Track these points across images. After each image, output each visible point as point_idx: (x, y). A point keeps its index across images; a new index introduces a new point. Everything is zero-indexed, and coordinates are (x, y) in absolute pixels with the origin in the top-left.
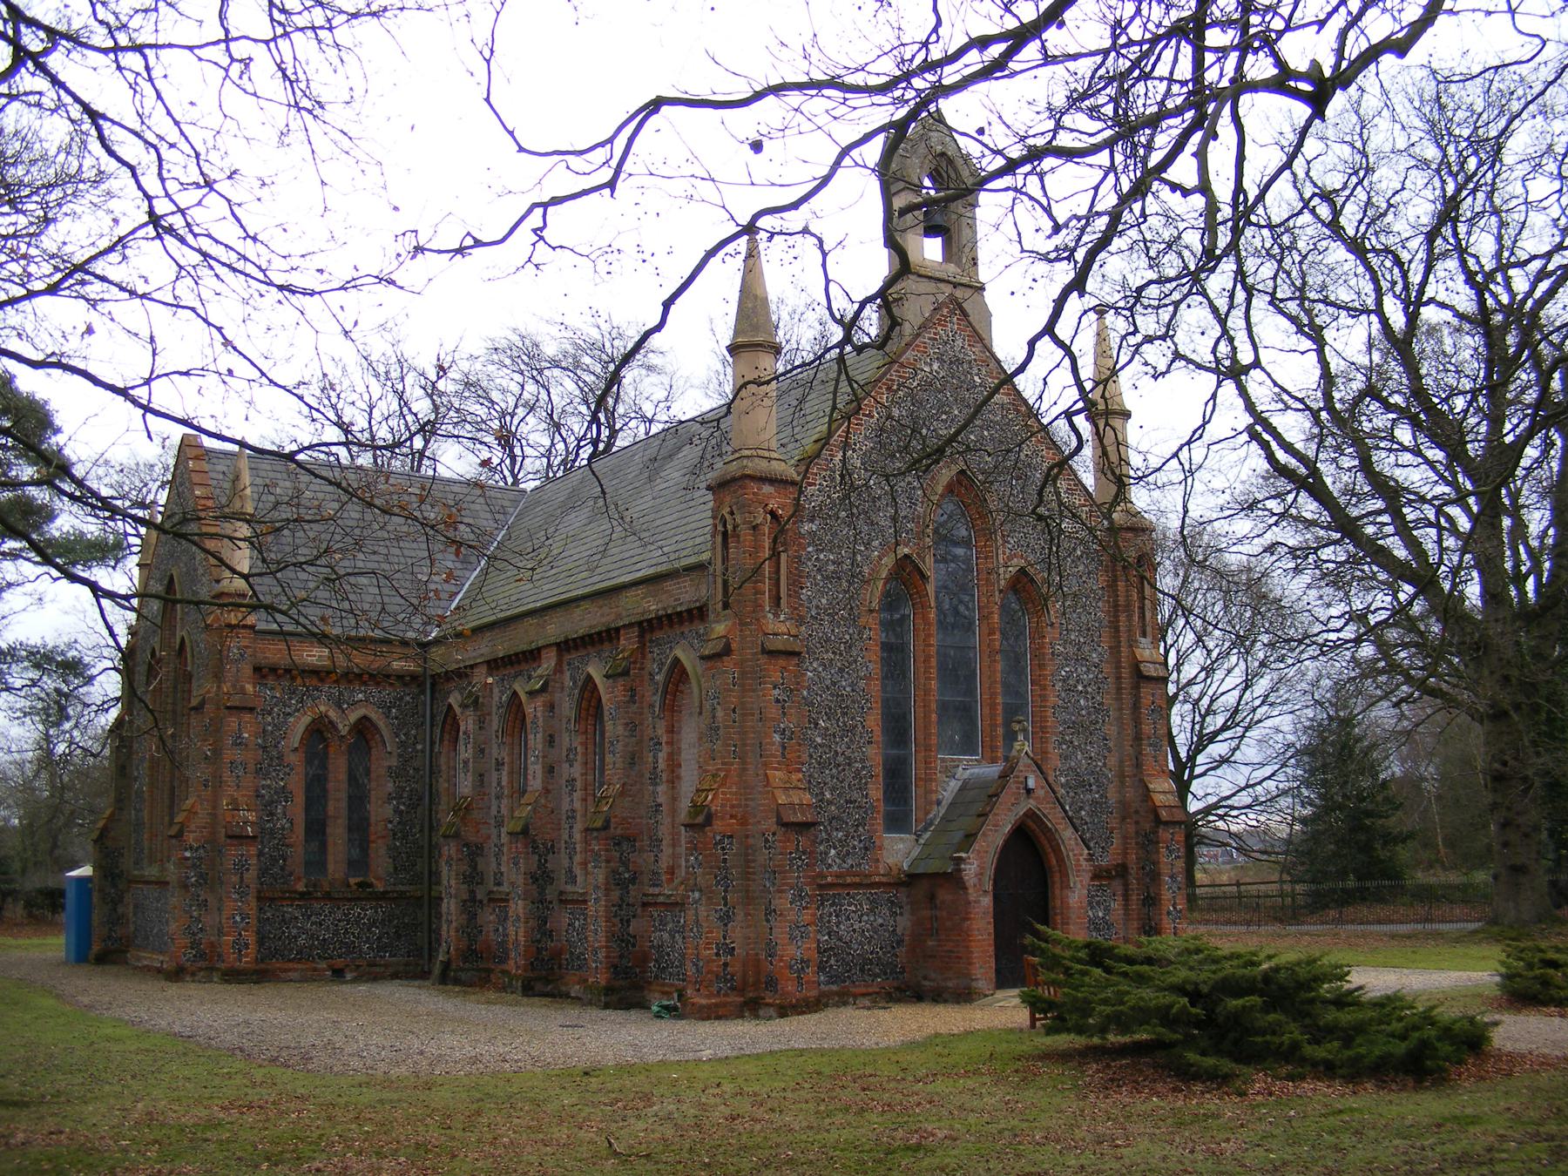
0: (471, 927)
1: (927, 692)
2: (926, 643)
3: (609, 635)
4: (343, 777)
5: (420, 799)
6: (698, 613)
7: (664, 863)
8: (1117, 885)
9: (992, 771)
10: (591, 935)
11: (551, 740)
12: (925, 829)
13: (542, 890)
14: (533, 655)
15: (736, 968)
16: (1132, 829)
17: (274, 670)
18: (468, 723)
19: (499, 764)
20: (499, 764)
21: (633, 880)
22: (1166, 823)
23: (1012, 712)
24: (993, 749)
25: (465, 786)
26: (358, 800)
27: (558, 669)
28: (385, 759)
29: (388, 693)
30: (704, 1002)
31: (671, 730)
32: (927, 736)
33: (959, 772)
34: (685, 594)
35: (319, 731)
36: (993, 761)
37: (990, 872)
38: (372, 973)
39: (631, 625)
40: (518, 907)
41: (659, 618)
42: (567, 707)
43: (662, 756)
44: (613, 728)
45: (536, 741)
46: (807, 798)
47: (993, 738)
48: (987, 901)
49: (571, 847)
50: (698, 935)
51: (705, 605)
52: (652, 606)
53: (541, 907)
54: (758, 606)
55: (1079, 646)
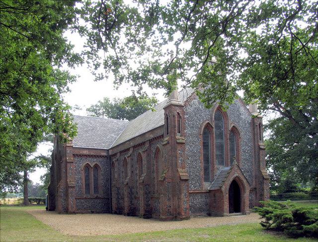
0: (118, 203)
1: (213, 152)
2: (214, 142)
3: (143, 143)
4: (92, 175)
5: (109, 180)
6: (162, 136)
7: (156, 189)
8: (254, 192)
9: (228, 168)
10: (141, 206)
11: (132, 166)
12: (213, 181)
13: (131, 196)
14: (128, 149)
15: (171, 210)
16: (257, 180)
17: (77, 155)
18: (116, 164)
19: (123, 172)
20: (123, 172)
21: (149, 193)
22: (265, 179)
23: (232, 156)
24: (228, 164)
25: (116, 176)
26: (96, 180)
27: (133, 152)
28: (102, 172)
29: (101, 159)
30: (164, 217)
31: (157, 162)
32: (213, 161)
33: (220, 169)
34: (159, 133)
35: (87, 167)
36: (228, 166)
37: (228, 189)
38: (63, 213)
39: (147, 141)
40: (126, 199)
41: (153, 138)
42: (135, 158)
43: (155, 167)
44: (144, 162)
45: (129, 166)
46: (187, 174)
47: (228, 162)
48: (228, 195)
49: (137, 187)
50: (164, 203)
51: (146, 110)
52: (152, 136)
53: (131, 199)
54: (175, 133)
55: (246, 142)
